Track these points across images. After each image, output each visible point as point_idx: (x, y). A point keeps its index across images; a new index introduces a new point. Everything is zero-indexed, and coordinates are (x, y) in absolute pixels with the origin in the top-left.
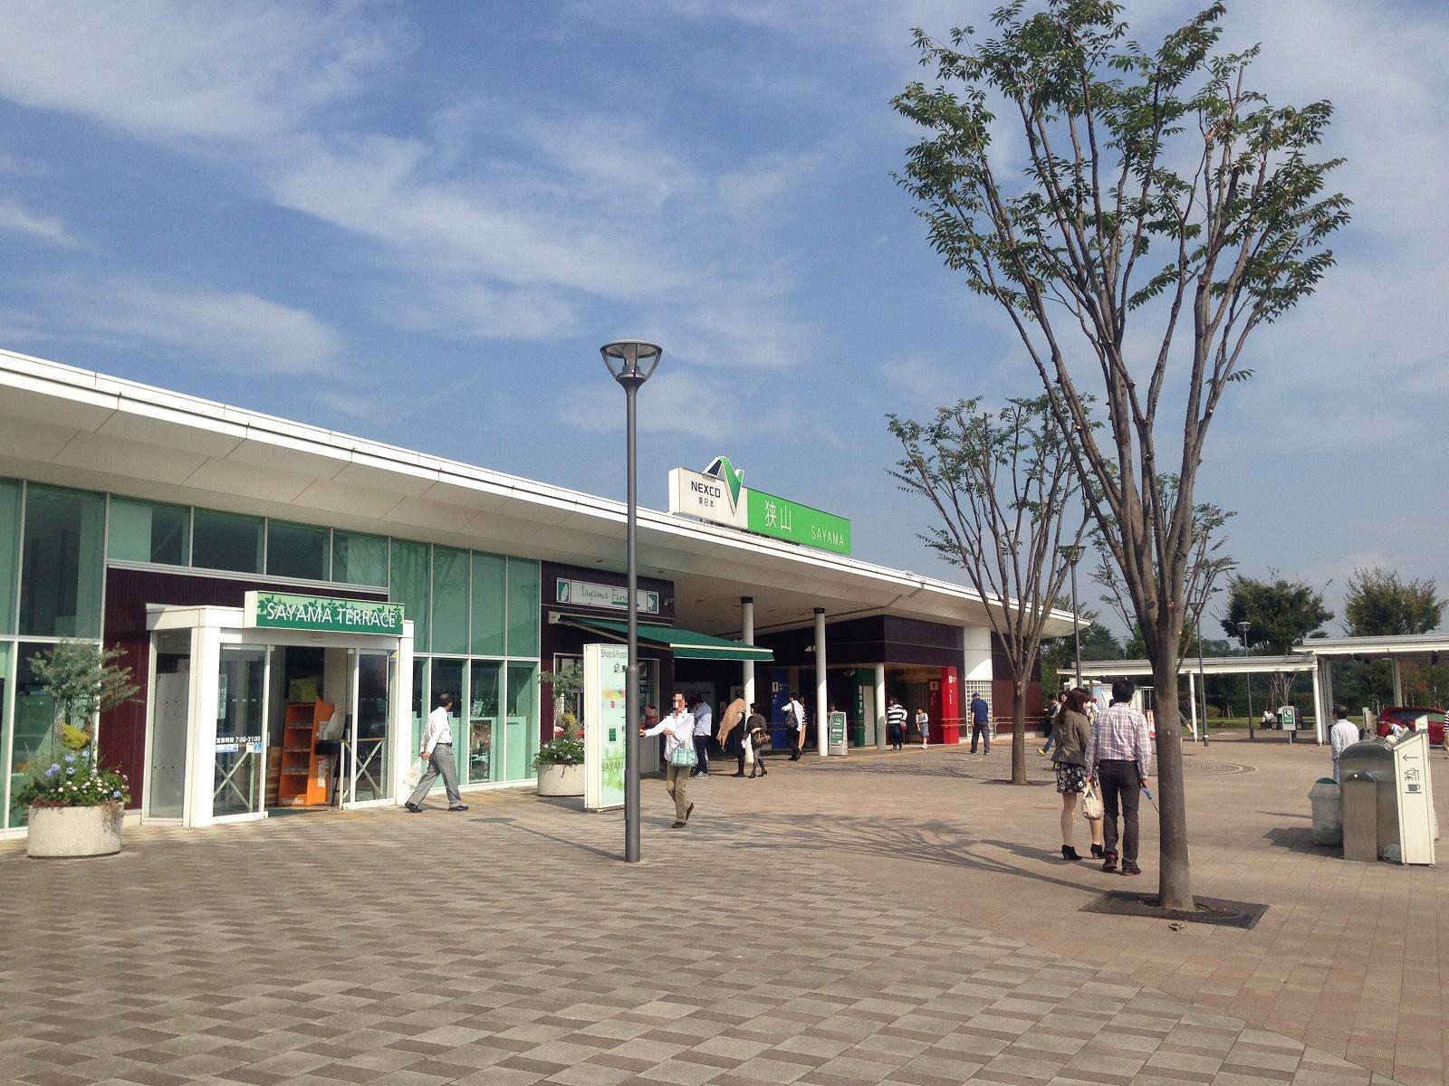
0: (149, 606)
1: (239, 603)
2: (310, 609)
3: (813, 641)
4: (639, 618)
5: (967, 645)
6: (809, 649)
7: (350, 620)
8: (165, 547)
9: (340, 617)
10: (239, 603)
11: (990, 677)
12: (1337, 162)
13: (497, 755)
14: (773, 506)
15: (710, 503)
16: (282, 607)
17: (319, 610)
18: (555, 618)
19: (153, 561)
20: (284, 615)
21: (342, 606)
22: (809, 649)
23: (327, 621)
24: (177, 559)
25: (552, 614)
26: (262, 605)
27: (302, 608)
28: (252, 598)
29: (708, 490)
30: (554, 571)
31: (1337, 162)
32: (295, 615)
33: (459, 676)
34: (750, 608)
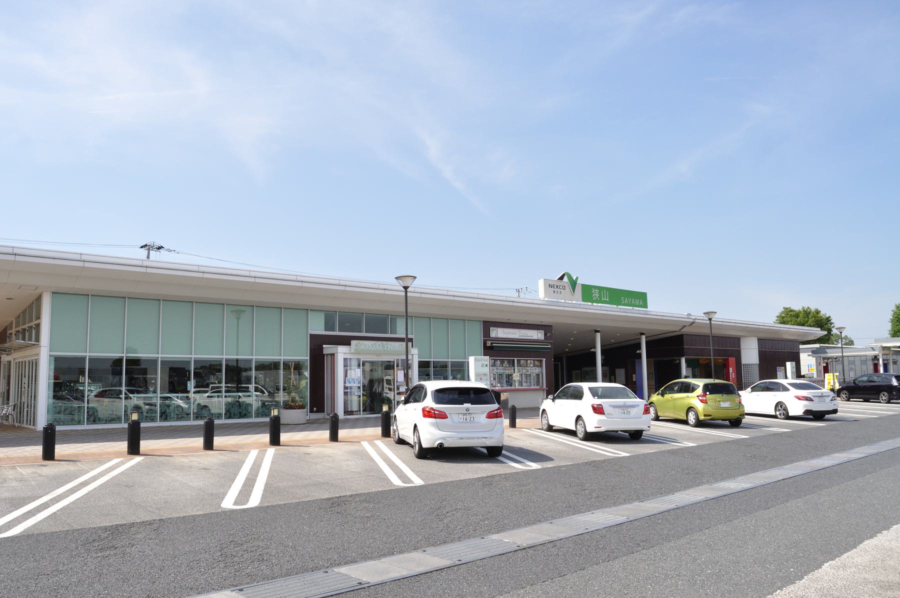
0: (324, 346)
1: (349, 344)
2: (374, 346)
3: (639, 348)
4: (36, 359)
5: (742, 346)
6: (638, 352)
7: (390, 349)
8: (329, 326)
9: (386, 348)
10: (349, 344)
11: (758, 362)
12: (8, 299)
13: (35, 381)
14: (597, 291)
15: (559, 292)
16: (363, 346)
17: (378, 346)
18: (489, 343)
19: (325, 330)
20: (364, 348)
21: (386, 344)
22: (638, 352)
23: (380, 350)
24: (334, 330)
25: (488, 342)
26: (356, 345)
27: (371, 346)
28: (353, 342)
29: (558, 287)
30: (488, 325)
31: (8, 299)
32: (368, 348)
33: (129, 368)
34: (598, 335)
